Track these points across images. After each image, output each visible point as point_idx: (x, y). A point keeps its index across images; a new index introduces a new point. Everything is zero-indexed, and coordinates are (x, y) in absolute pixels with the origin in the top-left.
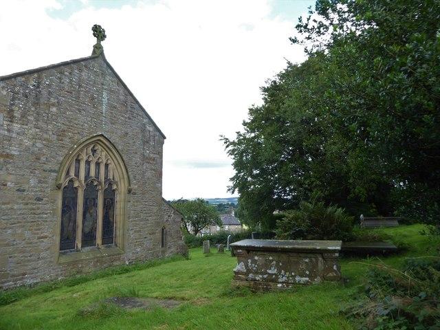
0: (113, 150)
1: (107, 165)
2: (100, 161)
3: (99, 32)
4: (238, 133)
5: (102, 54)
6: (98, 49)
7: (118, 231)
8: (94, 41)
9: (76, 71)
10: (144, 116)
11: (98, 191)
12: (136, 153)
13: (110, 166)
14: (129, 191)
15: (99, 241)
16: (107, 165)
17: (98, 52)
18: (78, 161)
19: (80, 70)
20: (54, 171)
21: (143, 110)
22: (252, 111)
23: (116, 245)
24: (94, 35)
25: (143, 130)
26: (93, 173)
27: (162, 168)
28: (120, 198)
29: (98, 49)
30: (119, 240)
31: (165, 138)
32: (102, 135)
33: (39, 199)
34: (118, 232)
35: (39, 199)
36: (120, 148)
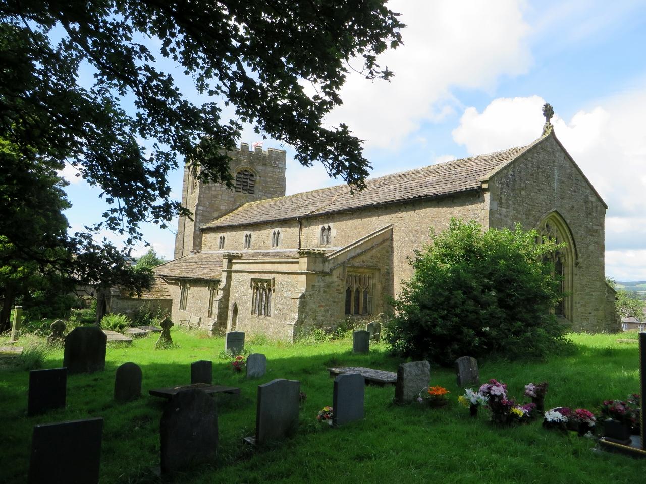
0: (564, 226)
5: (553, 132)
6: (549, 126)
9: (536, 155)
12: (581, 226)
17: (549, 131)
19: (538, 153)
23: (565, 316)
24: (544, 115)
29: (549, 126)
31: (606, 207)
36: (568, 222)
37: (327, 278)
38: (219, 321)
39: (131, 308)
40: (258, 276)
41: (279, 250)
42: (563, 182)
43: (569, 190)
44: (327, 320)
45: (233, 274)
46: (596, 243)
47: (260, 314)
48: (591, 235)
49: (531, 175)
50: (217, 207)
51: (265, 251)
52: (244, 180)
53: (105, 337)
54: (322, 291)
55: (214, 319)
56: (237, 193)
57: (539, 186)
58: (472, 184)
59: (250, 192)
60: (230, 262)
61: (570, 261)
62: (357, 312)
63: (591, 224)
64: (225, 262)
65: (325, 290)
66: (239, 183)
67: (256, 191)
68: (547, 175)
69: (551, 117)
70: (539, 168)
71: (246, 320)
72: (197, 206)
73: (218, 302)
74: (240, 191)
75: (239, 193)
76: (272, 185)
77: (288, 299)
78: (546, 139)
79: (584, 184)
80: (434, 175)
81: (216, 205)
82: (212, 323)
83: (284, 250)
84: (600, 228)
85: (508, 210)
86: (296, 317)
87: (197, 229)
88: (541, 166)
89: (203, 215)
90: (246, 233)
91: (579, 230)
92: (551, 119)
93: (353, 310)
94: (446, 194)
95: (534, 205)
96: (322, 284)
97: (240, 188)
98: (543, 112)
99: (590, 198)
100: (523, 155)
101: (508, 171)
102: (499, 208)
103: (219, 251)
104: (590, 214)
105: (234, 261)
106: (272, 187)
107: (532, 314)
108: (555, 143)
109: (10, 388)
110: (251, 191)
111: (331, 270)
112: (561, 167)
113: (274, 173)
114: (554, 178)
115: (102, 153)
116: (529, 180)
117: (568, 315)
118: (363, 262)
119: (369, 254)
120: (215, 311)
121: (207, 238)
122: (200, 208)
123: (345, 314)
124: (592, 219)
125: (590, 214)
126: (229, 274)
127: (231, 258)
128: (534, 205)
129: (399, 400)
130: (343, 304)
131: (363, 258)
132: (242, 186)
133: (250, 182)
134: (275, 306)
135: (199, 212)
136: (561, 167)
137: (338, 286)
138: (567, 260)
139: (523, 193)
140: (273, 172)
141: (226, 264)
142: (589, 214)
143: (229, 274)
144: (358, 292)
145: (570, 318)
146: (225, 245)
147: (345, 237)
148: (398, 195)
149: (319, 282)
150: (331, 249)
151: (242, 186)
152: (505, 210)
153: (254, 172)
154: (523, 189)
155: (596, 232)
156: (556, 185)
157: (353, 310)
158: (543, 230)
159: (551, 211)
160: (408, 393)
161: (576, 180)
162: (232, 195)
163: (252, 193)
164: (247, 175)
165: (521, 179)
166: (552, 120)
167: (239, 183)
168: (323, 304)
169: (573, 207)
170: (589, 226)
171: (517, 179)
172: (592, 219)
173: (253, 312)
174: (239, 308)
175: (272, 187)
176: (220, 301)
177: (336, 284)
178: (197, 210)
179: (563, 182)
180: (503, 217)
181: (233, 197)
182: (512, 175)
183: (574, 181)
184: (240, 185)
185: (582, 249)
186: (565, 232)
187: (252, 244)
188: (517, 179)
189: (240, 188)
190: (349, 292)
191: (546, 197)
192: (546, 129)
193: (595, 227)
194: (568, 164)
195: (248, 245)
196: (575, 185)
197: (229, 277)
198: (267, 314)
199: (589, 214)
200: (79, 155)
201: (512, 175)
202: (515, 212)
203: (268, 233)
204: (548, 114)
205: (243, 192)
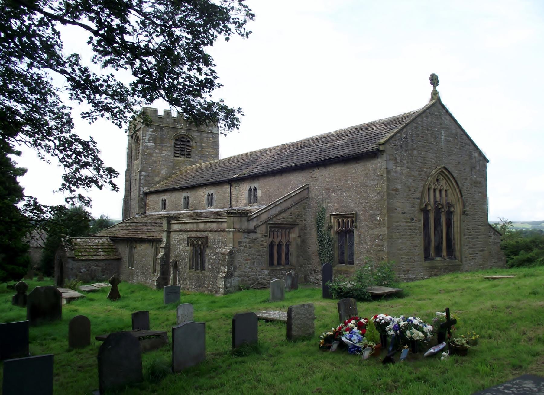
0: (452, 179)
1: (446, 191)
2: (442, 188)
3: (434, 80)
4: (91, 138)
5: (439, 99)
6: (435, 94)
7: (456, 246)
8: (431, 87)
9: (425, 119)
10: (471, 144)
11: (441, 213)
12: (466, 179)
13: (448, 192)
14: (464, 212)
15: (444, 253)
16: (446, 191)
17: (435, 98)
18: (429, 189)
19: (427, 117)
20: (418, 199)
21: (470, 139)
22: (66, 25)
23: (455, 258)
24: (431, 84)
25: (471, 157)
26: (438, 198)
27: (486, 190)
28: (456, 218)
29: (435, 94)
30: (457, 254)
31: (488, 161)
32: (444, 167)
33: (412, 219)
34: (457, 247)
35: (412, 219)
36: (455, 175)
37: (253, 236)
38: (162, 276)
39: (85, 268)
40: (193, 234)
41: (213, 210)
42: (450, 142)
43: (455, 148)
44: (253, 272)
45: (172, 233)
46: (480, 192)
47: (197, 269)
48: (475, 186)
49: (421, 137)
50: (158, 172)
51: (202, 211)
52: (181, 146)
53: (60, 294)
54: (248, 246)
55: (157, 275)
56: (175, 158)
57: (429, 146)
58: (372, 146)
59: (188, 156)
60: (169, 224)
61: (458, 209)
62: (279, 263)
63: (475, 176)
64: (165, 224)
65: (251, 245)
66: (177, 149)
67: (193, 155)
68: (435, 136)
69: (437, 85)
70: (428, 130)
71: (185, 275)
72: (140, 172)
73: (160, 260)
74: (178, 157)
75: (178, 158)
76: (207, 150)
77: (219, 254)
78: (433, 105)
79: (468, 142)
80: (343, 138)
81: (157, 170)
82: (155, 279)
83: (218, 210)
84: (483, 179)
85: (402, 168)
86: (226, 270)
87: (141, 193)
88: (430, 128)
89: (145, 180)
90: (184, 194)
91: (465, 182)
92: (437, 87)
93: (275, 262)
94: (350, 156)
95: (425, 163)
96: (247, 240)
97: (178, 153)
98: (430, 81)
99: (473, 153)
100: (413, 120)
101: (401, 134)
102: (394, 167)
103: (161, 213)
104: (474, 168)
105: (173, 222)
106: (207, 151)
107: (174, 304)
108: (441, 107)
109: (407, 288)
110: (188, 156)
111: (255, 228)
112: (447, 129)
113: (208, 139)
114: (442, 139)
115: (114, 6)
116: (420, 141)
117: (458, 257)
118: (283, 218)
119: (289, 212)
120: (158, 268)
121: (151, 199)
122: (143, 173)
123: (269, 265)
124: (475, 172)
125: (474, 168)
126: (169, 232)
127: (170, 219)
128: (425, 163)
129: (289, 336)
130: (267, 257)
131: (283, 215)
132: (179, 152)
133: (188, 148)
134: (209, 261)
135: (142, 177)
136: (447, 128)
137: (262, 241)
138: (456, 209)
139: (415, 152)
140: (207, 137)
141: (166, 224)
142: (473, 168)
143: (169, 232)
144: (280, 245)
145: (459, 259)
146: (166, 206)
147: (269, 197)
148: (312, 158)
149: (245, 238)
150: (257, 207)
151: (179, 152)
152: (400, 168)
153: (189, 138)
154: (415, 149)
155: (480, 183)
156: (443, 144)
157: (275, 262)
158: (434, 184)
159: (440, 167)
160: (295, 332)
161: (461, 139)
162: (172, 160)
163: (190, 158)
164: (184, 141)
165: (412, 140)
166: (438, 88)
167: (177, 149)
168: (250, 258)
169: (459, 163)
170: (473, 178)
171: (410, 141)
172: (475, 172)
173: (191, 268)
174: (179, 264)
175: (207, 151)
176: (162, 258)
177: (260, 240)
178: (140, 176)
179: (450, 142)
180: (398, 175)
181: (172, 162)
182: (404, 138)
183: (459, 139)
184: (178, 150)
185: (468, 199)
186: (452, 184)
187: (190, 205)
188: (410, 141)
189: (178, 153)
190: (271, 245)
191: (435, 155)
192: (433, 96)
193: (478, 179)
194: (453, 127)
195: (187, 206)
196: (460, 143)
197: (168, 237)
198: (203, 268)
199: (473, 168)
200: (19, 153)
201: (404, 138)
202: (408, 170)
203: (203, 193)
204: (434, 83)
205: (181, 157)
